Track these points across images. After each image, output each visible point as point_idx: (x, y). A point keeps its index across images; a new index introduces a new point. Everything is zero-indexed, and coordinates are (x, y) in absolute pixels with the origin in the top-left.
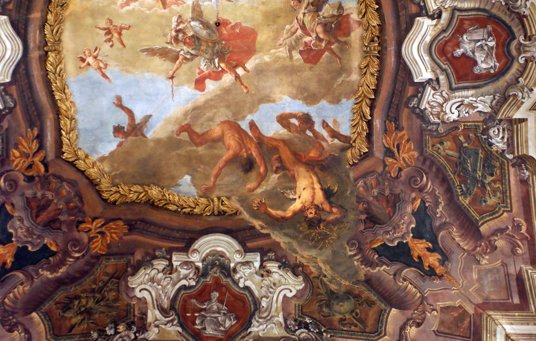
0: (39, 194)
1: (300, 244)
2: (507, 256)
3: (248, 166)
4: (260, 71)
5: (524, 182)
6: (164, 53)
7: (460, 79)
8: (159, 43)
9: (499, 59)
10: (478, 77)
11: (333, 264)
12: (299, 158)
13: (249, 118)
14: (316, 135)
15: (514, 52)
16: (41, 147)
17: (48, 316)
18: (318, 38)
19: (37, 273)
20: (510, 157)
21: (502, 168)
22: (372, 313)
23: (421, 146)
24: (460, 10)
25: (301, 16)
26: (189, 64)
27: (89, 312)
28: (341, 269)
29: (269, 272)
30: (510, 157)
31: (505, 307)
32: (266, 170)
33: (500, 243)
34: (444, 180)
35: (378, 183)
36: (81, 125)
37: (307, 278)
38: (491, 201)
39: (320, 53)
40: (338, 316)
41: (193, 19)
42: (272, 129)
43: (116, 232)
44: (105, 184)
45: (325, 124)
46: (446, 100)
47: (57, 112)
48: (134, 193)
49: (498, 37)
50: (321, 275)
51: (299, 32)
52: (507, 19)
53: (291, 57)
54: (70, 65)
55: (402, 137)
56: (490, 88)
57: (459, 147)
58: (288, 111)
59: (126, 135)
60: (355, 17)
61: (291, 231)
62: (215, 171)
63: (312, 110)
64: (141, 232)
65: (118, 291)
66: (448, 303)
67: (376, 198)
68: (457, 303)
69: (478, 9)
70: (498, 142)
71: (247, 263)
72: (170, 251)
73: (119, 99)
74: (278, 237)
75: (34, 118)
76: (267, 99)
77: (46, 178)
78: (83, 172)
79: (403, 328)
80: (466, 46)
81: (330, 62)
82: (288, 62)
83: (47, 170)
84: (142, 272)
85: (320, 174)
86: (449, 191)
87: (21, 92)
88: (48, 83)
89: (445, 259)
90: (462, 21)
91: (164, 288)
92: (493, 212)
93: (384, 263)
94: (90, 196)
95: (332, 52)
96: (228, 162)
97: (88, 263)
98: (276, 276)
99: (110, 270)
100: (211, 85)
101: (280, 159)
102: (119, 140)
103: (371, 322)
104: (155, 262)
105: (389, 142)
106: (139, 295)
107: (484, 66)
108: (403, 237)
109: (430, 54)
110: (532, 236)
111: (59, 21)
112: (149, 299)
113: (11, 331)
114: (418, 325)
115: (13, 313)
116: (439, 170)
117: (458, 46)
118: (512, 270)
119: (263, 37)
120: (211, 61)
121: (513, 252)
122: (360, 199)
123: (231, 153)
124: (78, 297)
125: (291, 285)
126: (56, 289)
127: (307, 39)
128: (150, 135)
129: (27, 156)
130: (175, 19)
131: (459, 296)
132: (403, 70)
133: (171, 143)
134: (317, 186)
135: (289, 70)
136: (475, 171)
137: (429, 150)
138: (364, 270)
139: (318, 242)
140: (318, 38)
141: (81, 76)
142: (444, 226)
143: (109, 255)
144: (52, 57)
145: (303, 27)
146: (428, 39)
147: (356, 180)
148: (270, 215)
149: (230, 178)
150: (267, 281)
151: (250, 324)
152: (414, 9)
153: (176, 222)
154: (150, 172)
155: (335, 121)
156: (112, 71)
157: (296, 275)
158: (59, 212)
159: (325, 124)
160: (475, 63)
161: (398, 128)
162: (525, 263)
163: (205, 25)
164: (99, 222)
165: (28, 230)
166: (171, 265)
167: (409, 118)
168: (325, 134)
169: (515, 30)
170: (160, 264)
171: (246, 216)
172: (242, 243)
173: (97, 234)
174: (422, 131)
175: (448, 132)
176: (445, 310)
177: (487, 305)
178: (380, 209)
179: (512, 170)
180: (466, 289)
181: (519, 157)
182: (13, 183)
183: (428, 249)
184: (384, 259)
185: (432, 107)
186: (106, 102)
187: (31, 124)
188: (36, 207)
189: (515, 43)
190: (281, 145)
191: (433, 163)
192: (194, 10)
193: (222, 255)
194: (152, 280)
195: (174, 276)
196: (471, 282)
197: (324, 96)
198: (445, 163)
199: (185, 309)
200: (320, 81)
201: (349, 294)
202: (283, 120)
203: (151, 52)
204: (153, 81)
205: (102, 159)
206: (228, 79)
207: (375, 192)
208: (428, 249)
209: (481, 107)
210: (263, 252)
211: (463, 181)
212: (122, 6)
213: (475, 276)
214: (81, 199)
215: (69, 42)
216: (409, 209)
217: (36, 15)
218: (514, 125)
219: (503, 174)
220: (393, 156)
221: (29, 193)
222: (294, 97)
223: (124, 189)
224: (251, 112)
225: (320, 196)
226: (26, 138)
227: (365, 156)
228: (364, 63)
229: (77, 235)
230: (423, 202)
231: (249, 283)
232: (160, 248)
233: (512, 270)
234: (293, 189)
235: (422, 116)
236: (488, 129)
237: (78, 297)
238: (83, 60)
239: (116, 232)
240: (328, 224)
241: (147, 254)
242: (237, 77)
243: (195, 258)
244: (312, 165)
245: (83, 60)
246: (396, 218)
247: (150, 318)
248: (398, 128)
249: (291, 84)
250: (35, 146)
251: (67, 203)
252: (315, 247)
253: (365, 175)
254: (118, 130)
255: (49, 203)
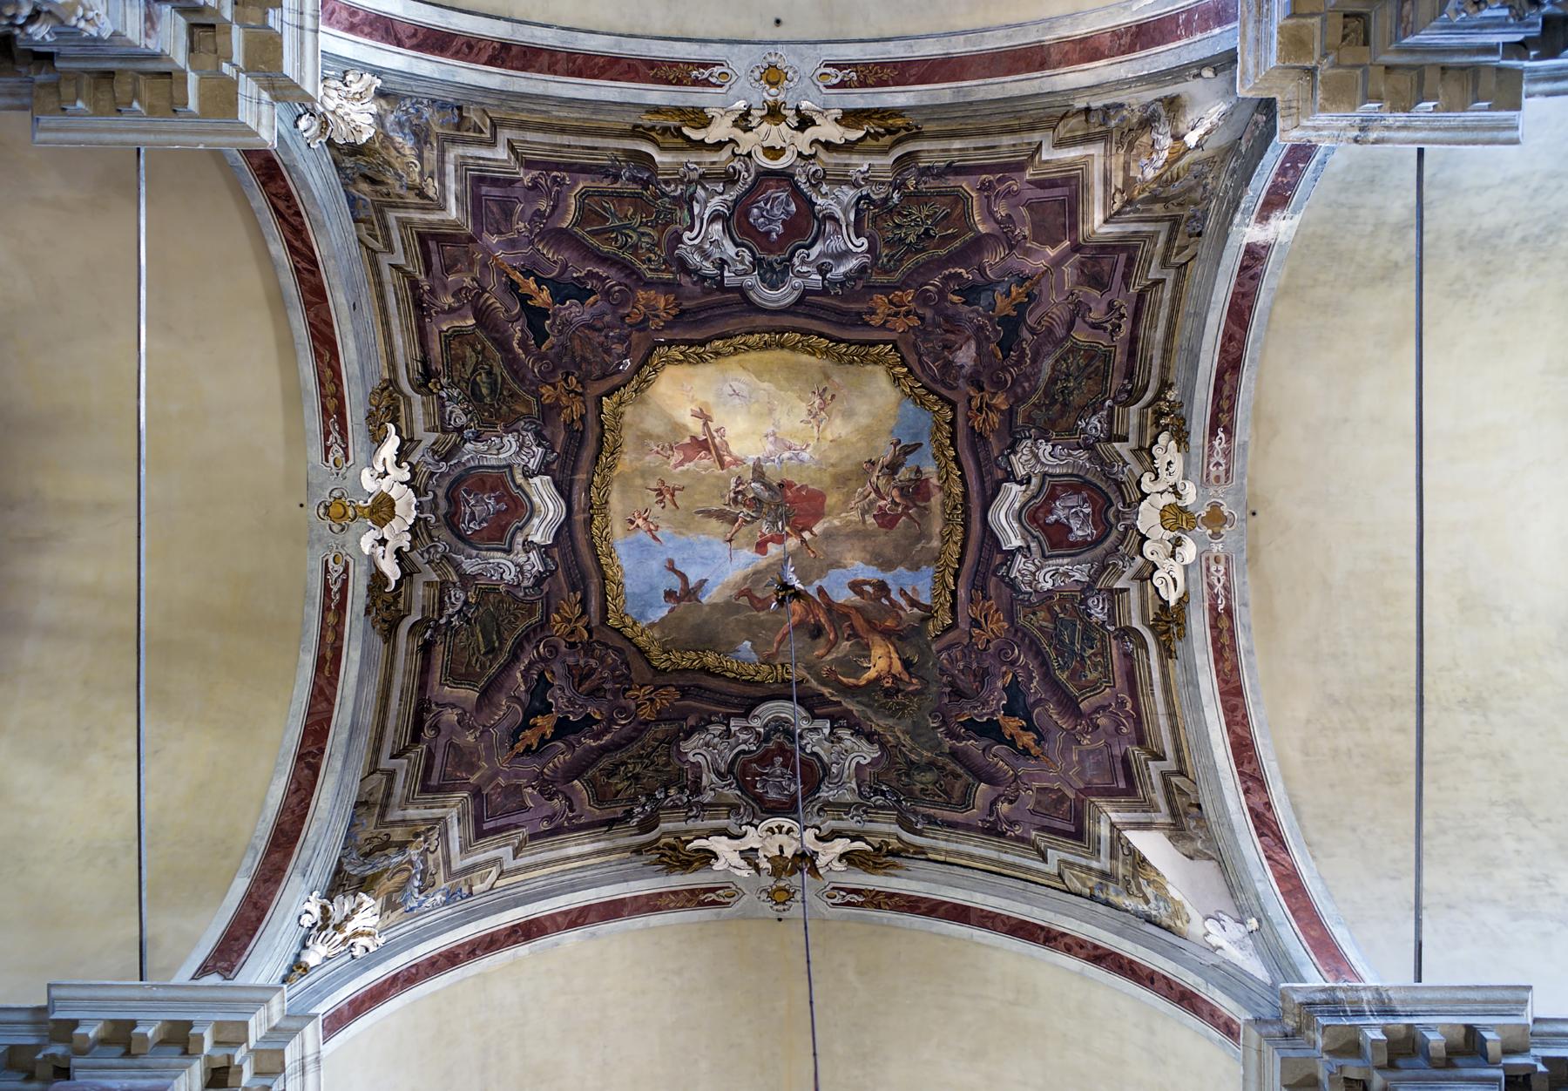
0: (582, 662)
1: (876, 713)
2: (1112, 736)
3: (817, 632)
4: (829, 535)
5: (1127, 655)
6: (721, 515)
7: (1053, 546)
8: (716, 505)
9: (1096, 527)
10: (1073, 545)
11: (913, 733)
12: (873, 627)
13: (817, 583)
14: (893, 603)
15: (1112, 520)
16: (584, 612)
17: (591, 783)
18: (893, 501)
19: (579, 742)
20: (1111, 628)
21: (1102, 639)
22: (958, 785)
23: (1011, 617)
24: (1051, 475)
25: (874, 479)
26: (750, 527)
27: (636, 778)
28: (923, 740)
29: (840, 739)
30: (1111, 628)
31: (1109, 793)
32: (836, 637)
33: (1102, 721)
34: (1039, 653)
35: (964, 655)
36: (628, 590)
37: (883, 746)
38: (1092, 676)
39: (898, 517)
40: (919, 786)
41: (754, 480)
42: (843, 596)
43: (668, 698)
44: (655, 651)
45: (903, 593)
46: (1039, 569)
47: (604, 577)
48: (688, 660)
49: (1094, 504)
50: (898, 745)
51: (873, 495)
52: (1103, 486)
53: (864, 522)
54: (617, 528)
55: (990, 607)
56: (1088, 556)
57: (1054, 617)
58: (861, 577)
59: (679, 600)
60: (934, 481)
61: (865, 700)
62: (778, 637)
63: (888, 577)
64: (694, 698)
65: (669, 756)
66: (1045, 784)
67: (962, 671)
68: (1056, 786)
69: (1071, 475)
70: (1098, 613)
71: (815, 730)
72: (728, 717)
73: (671, 562)
74: (849, 705)
75: (578, 582)
76: (836, 565)
77: (590, 644)
78: (630, 640)
79: (993, 803)
80: (1060, 513)
81: (908, 527)
82: (860, 526)
83: (590, 636)
84: (696, 736)
85: (898, 644)
86: (1044, 664)
87: (563, 556)
88: (593, 547)
89: (1041, 739)
90: (1054, 487)
91: (720, 753)
92: (1094, 687)
93: (971, 738)
94: (637, 663)
95: (910, 516)
96: (795, 627)
97: (635, 729)
98: (848, 743)
99: (660, 736)
100: (773, 549)
101: (852, 626)
102: (671, 605)
103: (957, 794)
104: (711, 727)
105: (974, 612)
106: (692, 760)
107: (1080, 533)
108: (993, 714)
109: (1020, 521)
110: (1139, 714)
111: (607, 483)
112: (703, 762)
113: (550, 799)
114: (1011, 802)
115: (552, 782)
116: (1032, 642)
117: (1051, 512)
118: (1117, 751)
119: (832, 500)
120: (774, 523)
121: (1117, 730)
122: (943, 672)
123: (796, 618)
124: (624, 763)
125: (867, 753)
126: (600, 756)
127: (882, 503)
128: (704, 600)
129: (569, 621)
130: (733, 480)
131: (1057, 779)
132: (990, 538)
133: (728, 608)
134: (894, 656)
135: (860, 534)
136: (1073, 643)
137: (1021, 621)
138: (948, 743)
139: (897, 712)
140: (893, 501)
141: (632, 537)
142: (1038, 702)
143: (658, 721)
144: (597, 521)
145: (877, 490)
146: (1017, 505)
147: (939, 652)
148: (841, 682)
149: (794, 645)
150: (837, 748)
151: (818, 789)
152: (1000, 474)
153: (735, 688)
154: (705, 640)
155: (914, 590)
156: (664, 531)
157: (871, 743)
158: (605, 680)
159: (903, 593)
160: (1071, 530)
161: (986, 598)
162: (1132, 744)
163: (768, 486)
164: (649, 689)
165: (569, 700)
166: (728, 730)
167: (997, 587)
168: (903, 602)
169: (1113, 497)
170: (717, 729)
171: (814, 683)
172: (809, 709)
173: (643, 701)
174: (1012, 600)
175: (1042, 602)
176: (1041, 790)
177: (1089, 790)
178: (965, 682)
179: (1114, 642)
180: (1066, 772)
181: (1121, 629)
182: (553, 649)
183: (1022, 728)
184: (971, 733)
185: (1023, 575)
186: (656, 565)
187: (574, 589)
188: (579, 676)
189: (1113, 509)
190: (853, 611)
191: (1025, 635)
192: (754, 470)
193: (787, 721)
194: (707, 745)
195: (732, 740)
196: (1070, 765)
197: (901, 563)
198: (1039, 635)
199: (744, 773)
200: (896, 548)
201: (931, 765)
202: (856, 586)
203: (708, 513)
204: (708, 543)
205: (652, 626)
206: (792, 543)
207: (961, 665)
208: (1022, 728)
209: (1078, 576)
210: (834, 720)
211: (1060, 654)
212: (676, 467)
213: (1075, 758)
214: (628, 667)
215: (616, 503)
216: (999, 684)
217: (581, 476)
218: (1114, 595)
219: (1104, 647)
220: (980, 627)
221: (571, 660)
222: (868, 563)
223: (675, 656)
224: (819, 577)
225: (897, 666)
226: (568, 602)
227: (947, 630)
228: (946, 531)
229: (623, 701)
230: (1015, 676)
231: (816, 749)
232: (716, 714)
233: (1117, 751)
234: (868, 657)
235: (1012, 585)
236: (1087, 599)
237: (624, 763)
238: (632, 522)
239: (668, 698)
240: (906, 695)
241: (702, 719)
242: (803, 541)
243: (756, 724)
244: (887, 634)
245: (632, 522)
246: (984, 694)
247: (705, 781)
248: (986, 598)
249: (864, 549)
250: (578, 610)
251: (613, 671)
252: (892, 716)
253: (949, 647)
254: (669, 595)
255: (592, 671)
